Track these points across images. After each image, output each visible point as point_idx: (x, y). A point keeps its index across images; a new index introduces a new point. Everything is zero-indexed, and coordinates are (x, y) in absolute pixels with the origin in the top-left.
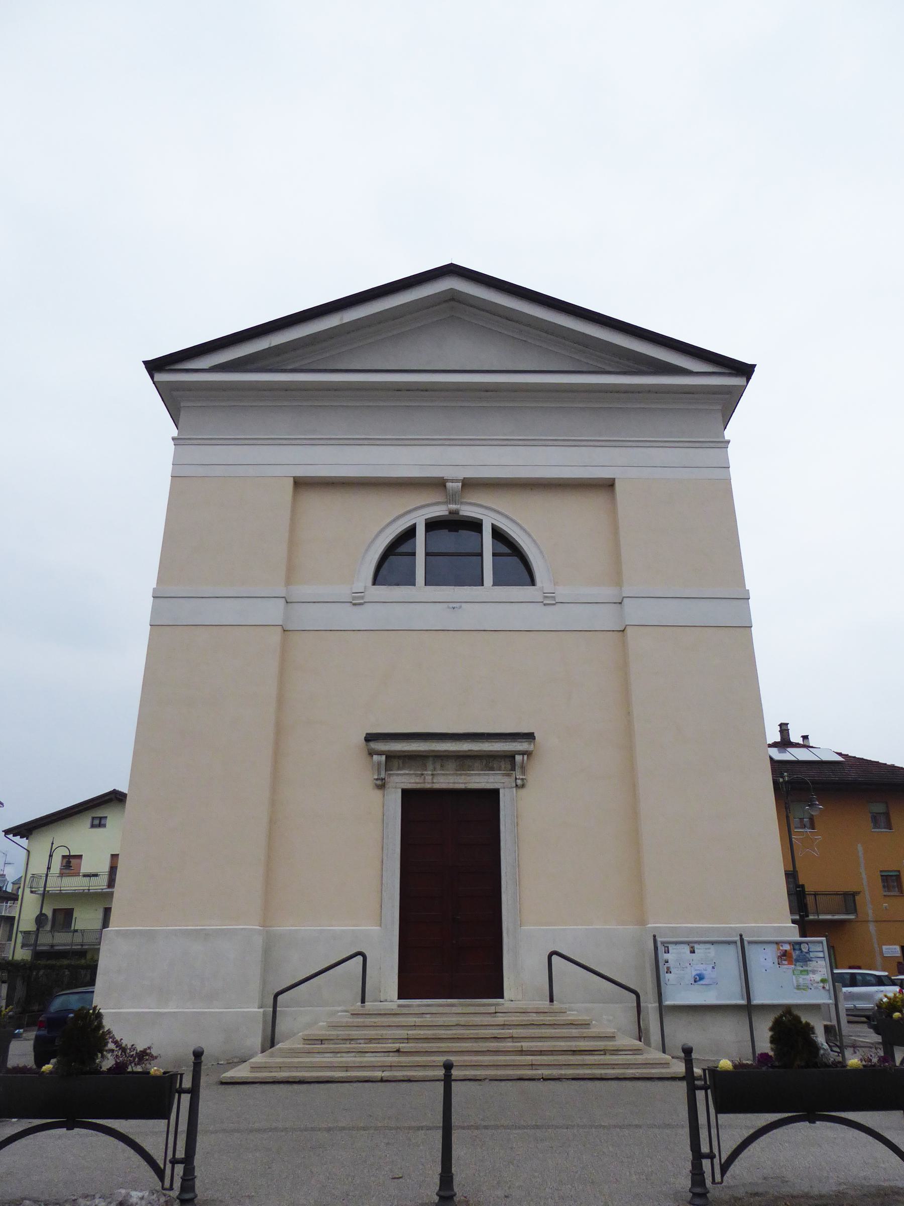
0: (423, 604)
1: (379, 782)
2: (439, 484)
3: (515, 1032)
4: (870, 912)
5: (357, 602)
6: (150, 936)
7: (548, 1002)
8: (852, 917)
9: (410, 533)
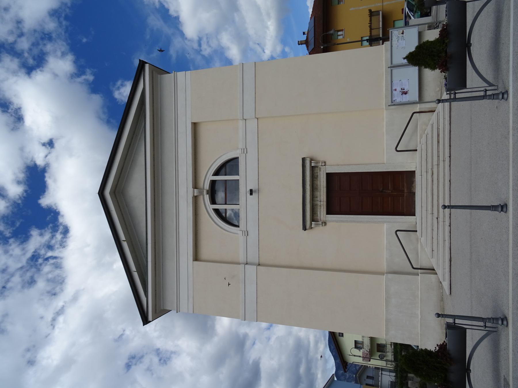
0: (246, 206)
1: (323, 224)
2: (195, 199)
3: (430, 167)
4: (379, 4)
5: (247, 233)
6: (388, 321)
7: (417, 152)
8: (381, 13)
9: (217, 211)
